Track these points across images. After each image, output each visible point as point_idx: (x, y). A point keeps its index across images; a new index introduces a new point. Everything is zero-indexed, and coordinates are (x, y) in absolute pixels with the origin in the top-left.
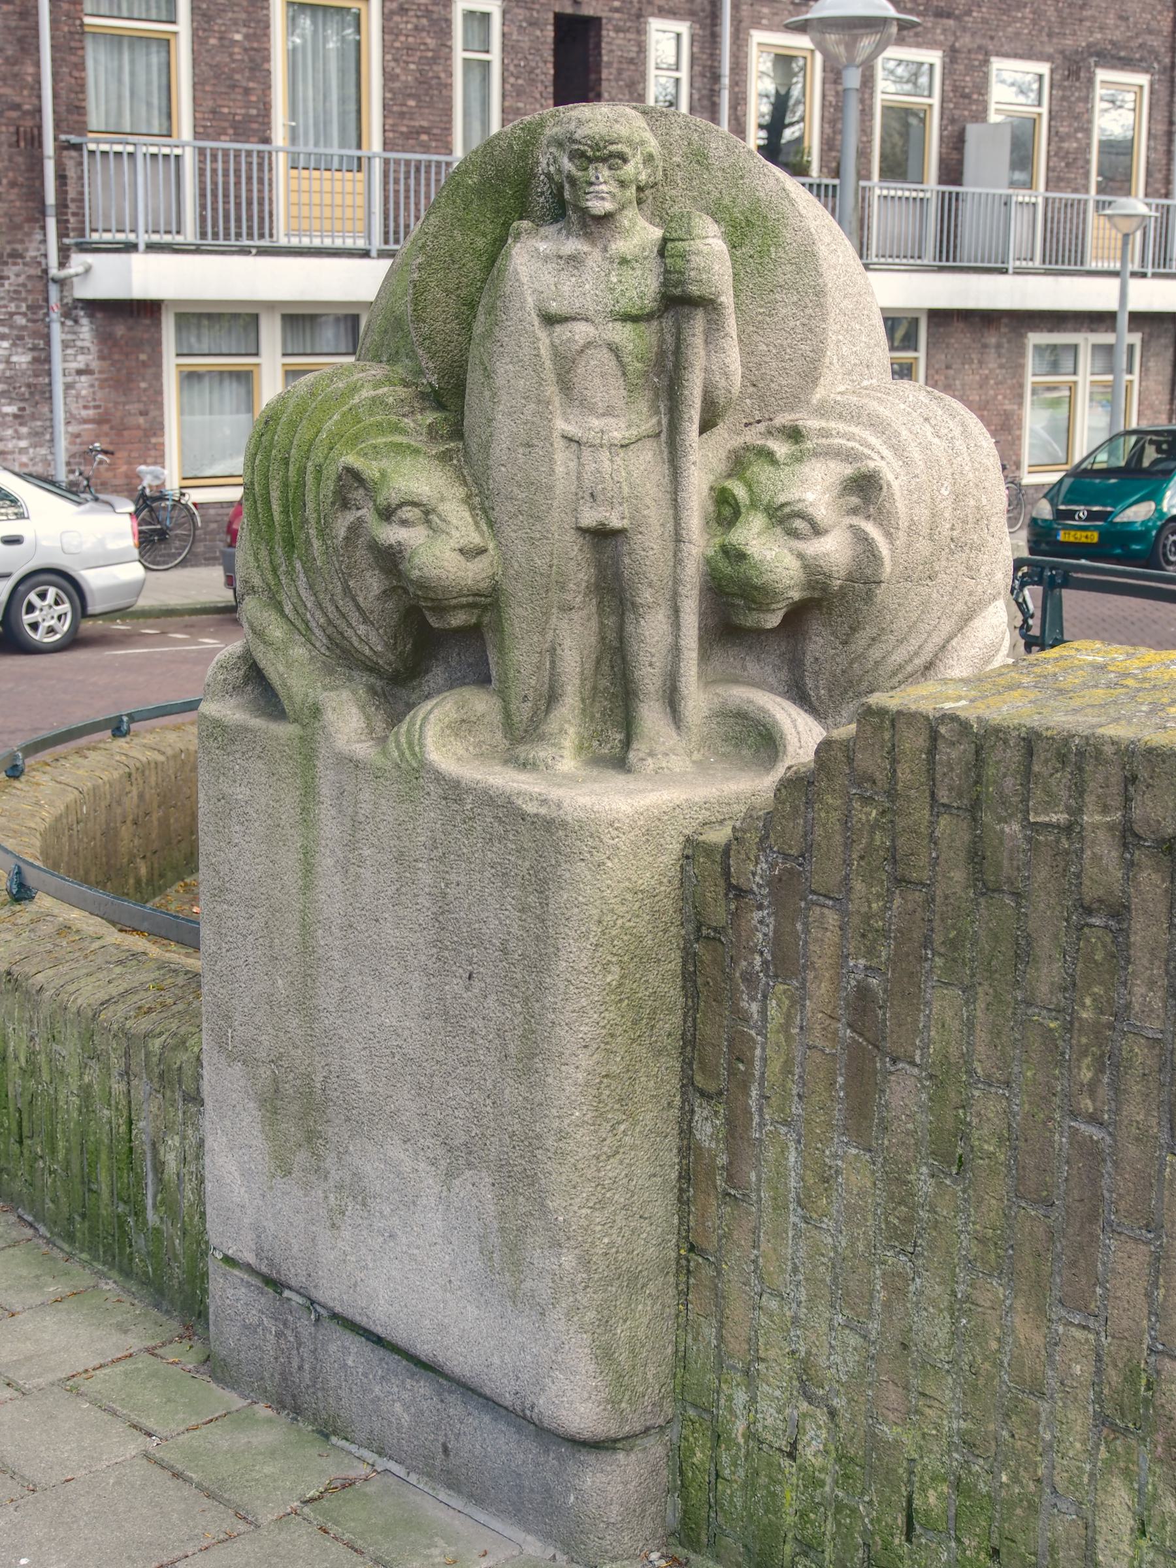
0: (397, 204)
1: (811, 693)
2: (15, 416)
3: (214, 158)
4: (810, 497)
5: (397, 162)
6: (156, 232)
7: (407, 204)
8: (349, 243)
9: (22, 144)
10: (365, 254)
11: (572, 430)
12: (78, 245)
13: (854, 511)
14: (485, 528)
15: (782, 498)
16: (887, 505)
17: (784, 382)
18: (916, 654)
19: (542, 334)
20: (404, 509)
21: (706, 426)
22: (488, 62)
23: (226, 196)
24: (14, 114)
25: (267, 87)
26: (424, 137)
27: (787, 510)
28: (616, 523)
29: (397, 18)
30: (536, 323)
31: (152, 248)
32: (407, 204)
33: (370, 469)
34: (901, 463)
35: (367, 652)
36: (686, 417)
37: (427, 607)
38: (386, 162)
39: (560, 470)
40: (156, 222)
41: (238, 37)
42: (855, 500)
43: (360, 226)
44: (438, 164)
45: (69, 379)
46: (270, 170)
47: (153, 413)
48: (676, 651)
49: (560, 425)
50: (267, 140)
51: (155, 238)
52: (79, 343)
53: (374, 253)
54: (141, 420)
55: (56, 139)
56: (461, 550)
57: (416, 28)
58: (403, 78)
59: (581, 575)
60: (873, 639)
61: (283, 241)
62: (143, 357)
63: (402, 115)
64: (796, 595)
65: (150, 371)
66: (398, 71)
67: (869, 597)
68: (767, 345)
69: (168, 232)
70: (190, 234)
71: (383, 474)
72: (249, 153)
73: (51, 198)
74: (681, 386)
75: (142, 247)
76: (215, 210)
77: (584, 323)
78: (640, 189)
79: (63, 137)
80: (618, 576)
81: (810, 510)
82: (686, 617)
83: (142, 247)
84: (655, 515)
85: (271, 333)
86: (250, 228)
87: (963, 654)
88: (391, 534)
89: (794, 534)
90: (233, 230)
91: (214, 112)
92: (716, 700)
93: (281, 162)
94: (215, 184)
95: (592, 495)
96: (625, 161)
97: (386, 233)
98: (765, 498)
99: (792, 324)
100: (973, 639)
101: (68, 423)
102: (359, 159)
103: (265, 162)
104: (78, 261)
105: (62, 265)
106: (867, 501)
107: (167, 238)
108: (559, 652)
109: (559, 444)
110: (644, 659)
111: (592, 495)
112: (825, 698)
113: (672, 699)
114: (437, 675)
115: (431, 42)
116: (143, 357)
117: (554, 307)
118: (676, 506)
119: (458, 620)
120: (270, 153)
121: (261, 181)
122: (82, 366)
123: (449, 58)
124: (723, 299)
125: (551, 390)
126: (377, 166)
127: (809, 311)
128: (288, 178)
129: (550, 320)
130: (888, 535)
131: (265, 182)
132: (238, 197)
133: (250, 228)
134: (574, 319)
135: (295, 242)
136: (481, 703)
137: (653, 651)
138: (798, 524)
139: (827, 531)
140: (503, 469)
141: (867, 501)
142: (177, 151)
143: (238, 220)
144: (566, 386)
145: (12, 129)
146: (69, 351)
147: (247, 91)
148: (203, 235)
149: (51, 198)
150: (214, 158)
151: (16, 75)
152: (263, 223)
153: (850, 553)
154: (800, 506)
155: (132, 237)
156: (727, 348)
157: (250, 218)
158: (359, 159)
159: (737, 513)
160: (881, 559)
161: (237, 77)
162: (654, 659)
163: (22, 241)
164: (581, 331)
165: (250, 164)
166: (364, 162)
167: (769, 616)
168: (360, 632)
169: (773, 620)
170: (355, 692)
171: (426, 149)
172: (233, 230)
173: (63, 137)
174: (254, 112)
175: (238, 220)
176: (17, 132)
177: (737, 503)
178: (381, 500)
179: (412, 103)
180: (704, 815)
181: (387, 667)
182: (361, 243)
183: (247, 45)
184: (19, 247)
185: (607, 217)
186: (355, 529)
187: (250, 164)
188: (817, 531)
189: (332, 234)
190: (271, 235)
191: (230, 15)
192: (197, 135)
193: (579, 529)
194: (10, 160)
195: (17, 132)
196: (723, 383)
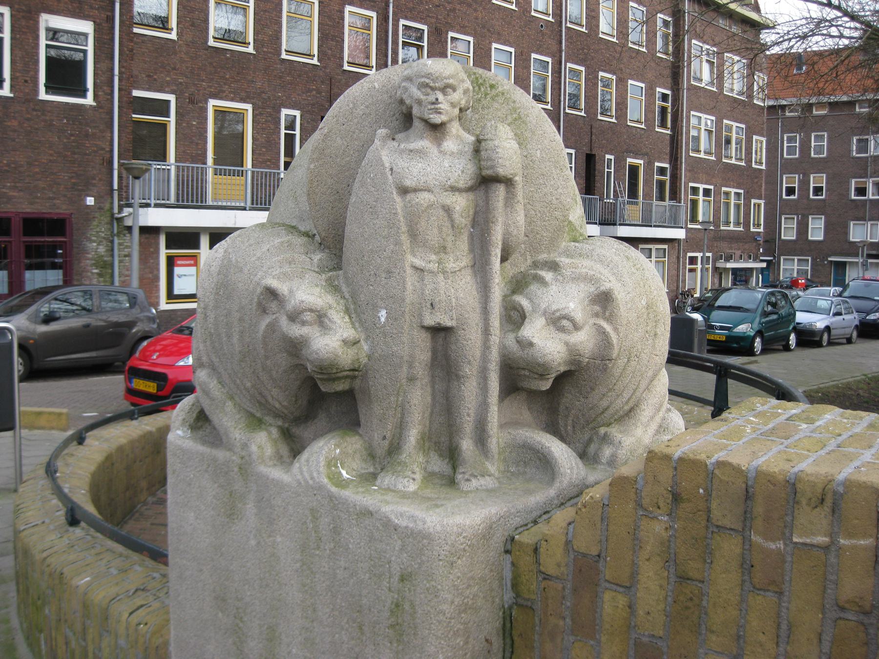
0: (257, 189)
1: (562, 429)
2: (98, 274)
3: (183, 170)
4: (572, 305)
5: (258, 172)
6: (158, 199)
7: (261, 189)
8: (238, 204)
9: (105, 164)
10: (244, 209)
11: (418, 262)
12: (126, 204)
13: (597, 315)
14: (357, 324)
15: (554, 307)
16: (615, 311)
17: (545, 234)
18: (627, 402)
19: (398, 199)
20: (305, 314)
21: (504, 259)
22: (295, 134)
23: (188, 185)
24: (102, 152)
25: (206, 142)
26: (268, 163)
27: (558, 314)
28: (449, 323)
29: (258, 117)
30: (395, 193)
31: (157, 206)
32: (261, 189)
33: (282, 287)
34: (620, 285)
35: (277, 405)
36: (493, 254)
37: (321, 379)
38: (253, 172)
39: (409, 287)
40: (158, 195)
41: (194, 123)
42: (597, 308)
43: (243, 197)
44: (274, 173)
45: (121, 258)
46: (206, 175)
47: (155, 272)
48: (484, 406)
49: (410, 259)
50: (205, 163)
51: (158, 202)
52: (125, 244)
53: (248, 209)
54: (150, 276)
55: (119, 162)
56: (343, 341)
57: (266, 121)
58: (260, 140)
59: (423, 355)
60: (604, 395)
61: (211, 203)
62: (152, 250)
63: (260, 154)
64: (562, 369)
65: (155, 256)
66: (259, 137)
67: (605, 369)
68: (535, 211)
69: (163, 200)
70: (173, 200)
71: (291, 291)
72: (197, 168)
73: (116, 187)
74: (489, 234)
75: (153, 205)
76: (183, 191)
77: (426, 193)
78: (461, 110)
79: (122, 161)
80: (447, 357)
81: (572, 314)
82: (492, 384)
83: (153, 205)
84: (474, 318)
85: (204, 241)
86: (197, 198)
87: (650, 402)
88: (296, 331)
89: (562, 329)
90: (190, 199)
91: (184, 152)
92: (509, 437)
93: (210, 172)
94: (183, 181)
95: (432, 304)
96: (454, 90)
97: (253, 200)
98: (543, 306)
99: (550, 198)
100: (654, 392)
101: (120, 277)
102: (242, 171)
103: (204, 171)
104: (127, 211)
105: (119, 212)
106: (604, 308)
107: (163, 202)
108: (407, 406)
109: (409, 271)
110: (464, 412)
111: (432, 304)
112: (570, 432)
113: (481, 438)
114: (321, 421)
115: (272, 127)
116: (152, 250)
117: (408, 183)
118: (485, 311)
119: (341, 386)
120: (206, 168)
121: (202, 180)
122: (127, 253)
123: (279, 133)
124: (517, 178)
125: (404, 238)
126: (249, 173)
127: (560, 191)
128: (213, 178)
129: (404, 191)
130: (616, 329)
131: (204, 181)
132: (192, 186)
133: (197, 198)
134: (421, 190)
135: (215, 204)
136: (354, 443)
137: (470, 406)
138: (565, 323)
139: (582, 327)
140: (371, 288)
141: (604, 308)
142: (168, 167)
143: (192, 195)
144: (413, 235)
145: (101, 158)
146: (121, 247)
147: (197, 144)
148: (178, 201)
149: (116, 187)
150: (183, 170)
151: (104, 137)
152: (203, 196)
153: (593, 341)
154: (566, 311)
155: (149, 201)
156: (518, 210)
157: (197, 194)
158: (242, 171)
159: (523, 317)
160: (613, 345)
161: (194, 138)
162: (470, 411)
163: (103, 203)
164: (424, 198)
165: (197, 173)
166: (244, 172)
167: (544, 383)
168: (272, 393)
169: (546, 385)
170: (270, 433)
171: (269, 168)
172: (190, 199)
173: (122, 161)
174: (200, 152)
175: (192, 195)
176: (103, 159)
177: (523, 311)
178: (290, 307)
179: (264, 150)
180: (518, 521)
181: (290, 415)
182: (242, 205)
183: (198, 126)
184: (102, 205)
185: (443, 124)
186: (272, 327)
187: (197, 173)
188: (577, 327)
189: (230, 200)
190: (206, 201)
191: (192, 114)
192: (176, 161)
193: (423, 327)
194: (100, 170)
195: (103, 159)
196: (515, 232)
